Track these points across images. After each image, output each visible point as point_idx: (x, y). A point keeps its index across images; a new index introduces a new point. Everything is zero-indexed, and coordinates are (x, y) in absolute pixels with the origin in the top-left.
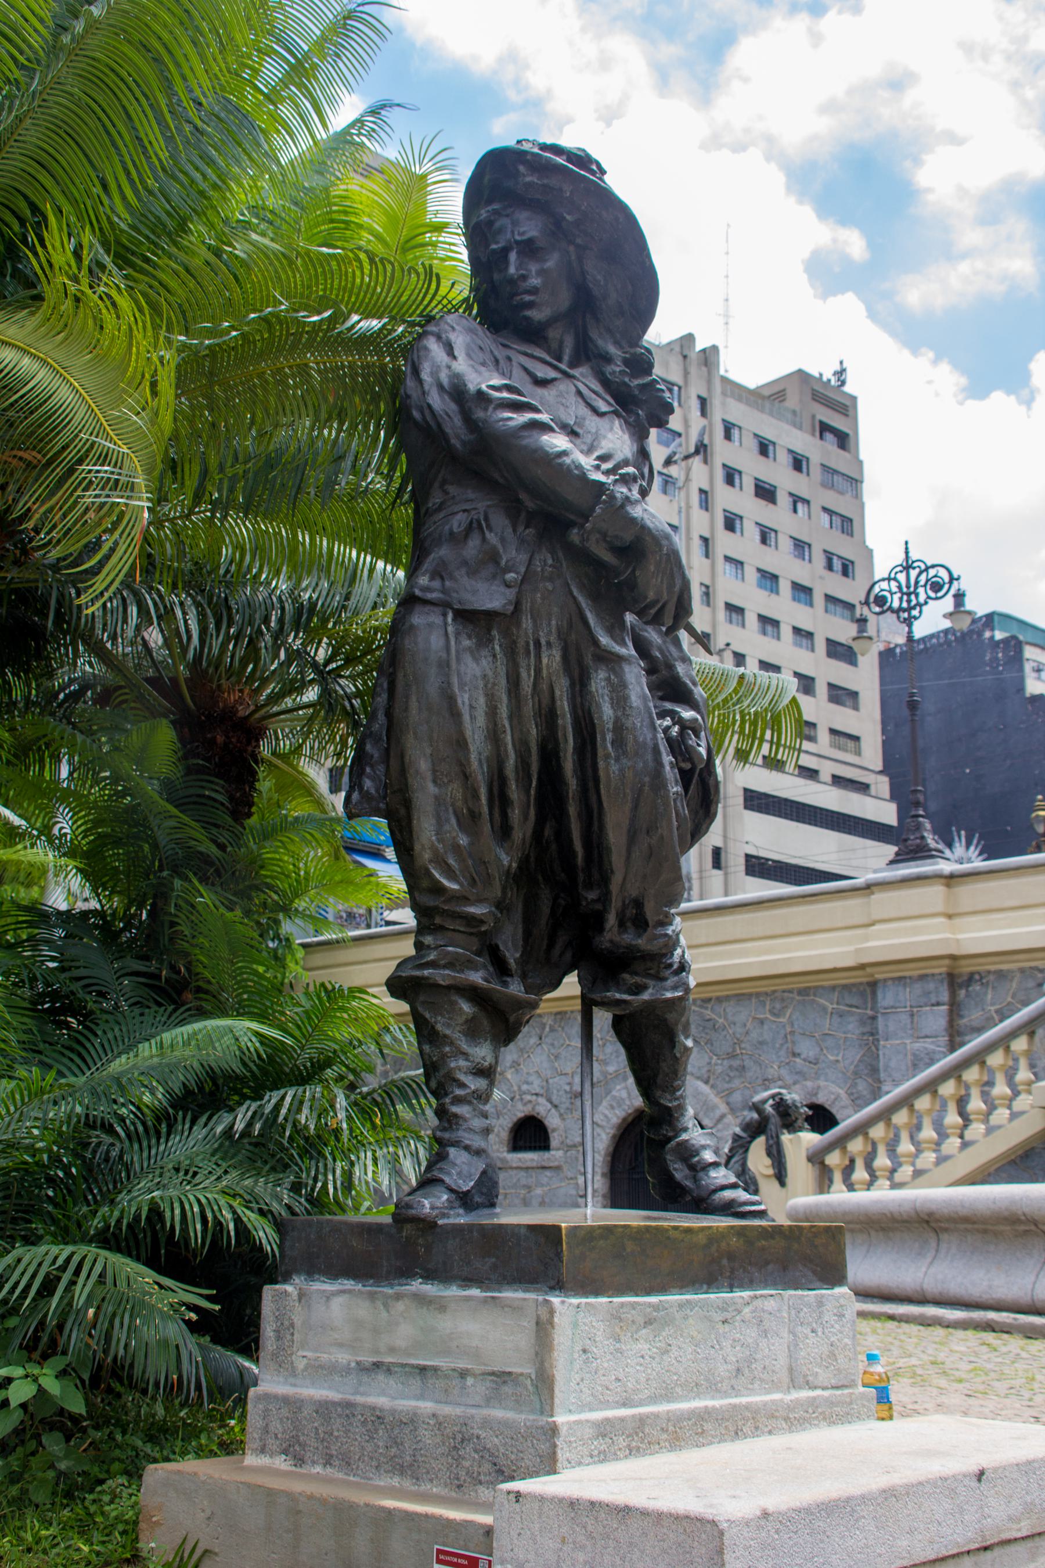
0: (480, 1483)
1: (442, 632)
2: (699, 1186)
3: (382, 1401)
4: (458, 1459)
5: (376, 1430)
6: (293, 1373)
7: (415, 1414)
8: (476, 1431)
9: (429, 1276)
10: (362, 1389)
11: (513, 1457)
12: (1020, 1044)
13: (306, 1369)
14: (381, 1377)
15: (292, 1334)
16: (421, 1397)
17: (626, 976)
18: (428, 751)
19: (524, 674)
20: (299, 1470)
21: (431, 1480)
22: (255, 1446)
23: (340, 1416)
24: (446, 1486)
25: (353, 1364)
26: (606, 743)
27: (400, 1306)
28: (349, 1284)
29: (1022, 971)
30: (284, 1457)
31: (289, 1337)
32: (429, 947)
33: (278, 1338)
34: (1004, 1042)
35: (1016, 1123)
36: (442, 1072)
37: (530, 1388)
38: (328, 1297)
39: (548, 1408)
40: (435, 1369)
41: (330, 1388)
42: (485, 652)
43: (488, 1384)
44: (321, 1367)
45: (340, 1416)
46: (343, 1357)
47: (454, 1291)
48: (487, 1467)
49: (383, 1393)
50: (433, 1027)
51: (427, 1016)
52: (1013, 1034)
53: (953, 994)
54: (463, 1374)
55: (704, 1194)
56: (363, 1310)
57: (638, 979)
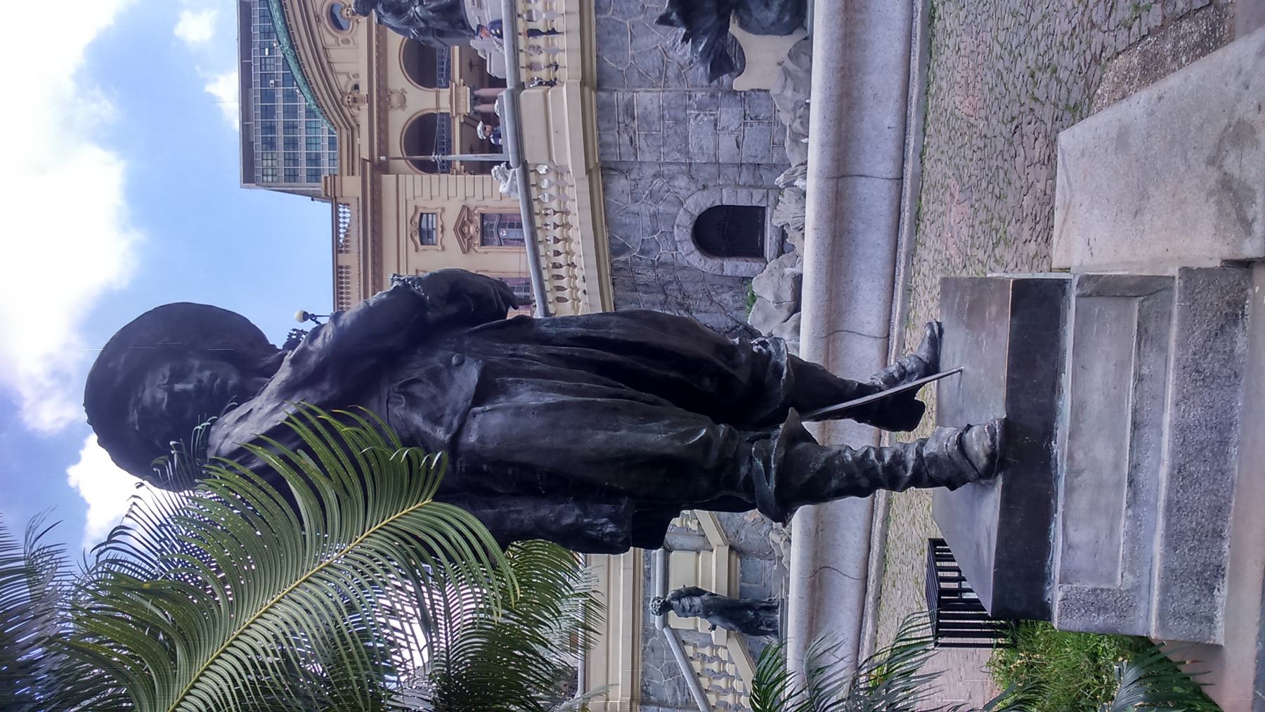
0: (1232, 351)
1: (488, 414)
2: (918, 369)
3: (1164, 472)
4: (1215, 377)
5: (1191, 474)
6: (1136, 588)
7: (1176, 426)
8: (1190, 356)
9: (1048, 433)
10: (1152, 500)
11: (1210, 315)
12: (690, 650)
13: (1133, 572)
14: (1141, 476)
15: (1102, 590)
16: (1159, 426)
17: (767, 379)
18: (590, 431)
19: (536, 368)
20: (1227, 572)
21: (1232, 408)
22: (1207, 630)
23: (1179, 520)
24: (1235, 391)
25: (1130, 512)
26: (594, 333)
27: (1079, 455)
28: (1057, 529)
29: (643, 660)
30: (1216, 592)
31: (1104, 595)
32: (750, 470)
33: (1105, 610)
34: (688, 660)
35: (734, 659)
36: (856, 470)
37: (1151, 301)
38: (1068, 546)
39: (1167, 282)
40: (1135, 412)
41: (1151, 541)
42: (512, 390)
43: (1148, 349)
44: (1132, 554)
45: (1179, 520)
46: (1123, 525)
47: (1065, 404)
48: (1219, 344)
49: (1156, 472)
50: (818, 472)
51: (808, 476)
52: (684, 653)
53: (653, 703)
54: (1140, 379)
55: (922, 366)
56: (1082, 501)
57: (770, 370)
